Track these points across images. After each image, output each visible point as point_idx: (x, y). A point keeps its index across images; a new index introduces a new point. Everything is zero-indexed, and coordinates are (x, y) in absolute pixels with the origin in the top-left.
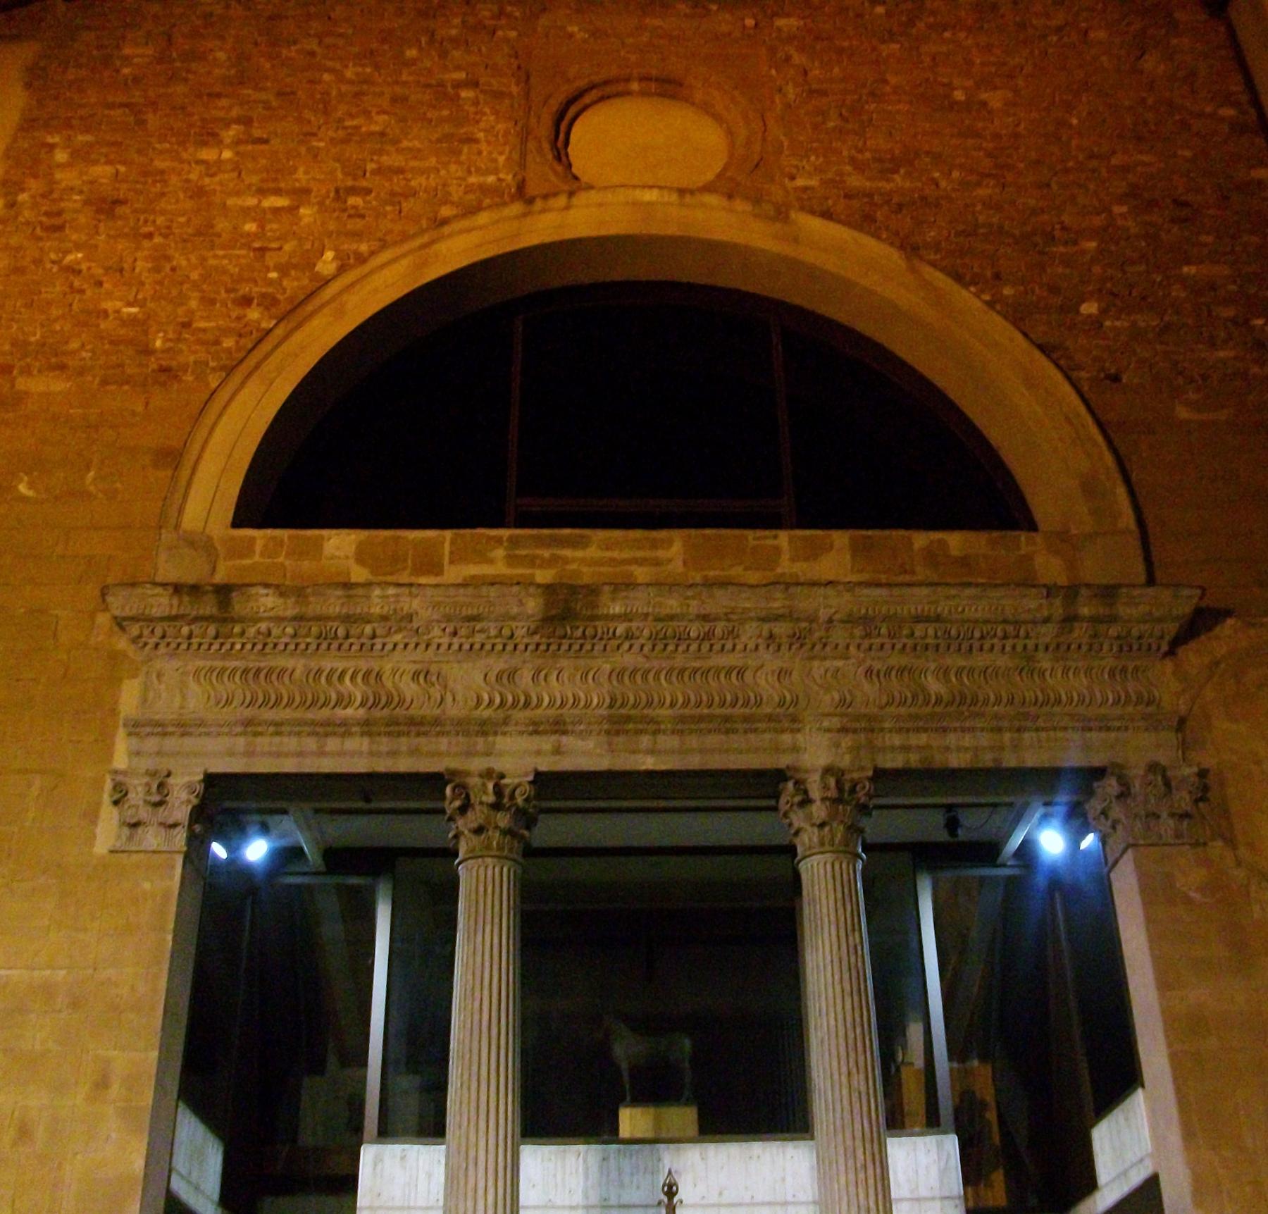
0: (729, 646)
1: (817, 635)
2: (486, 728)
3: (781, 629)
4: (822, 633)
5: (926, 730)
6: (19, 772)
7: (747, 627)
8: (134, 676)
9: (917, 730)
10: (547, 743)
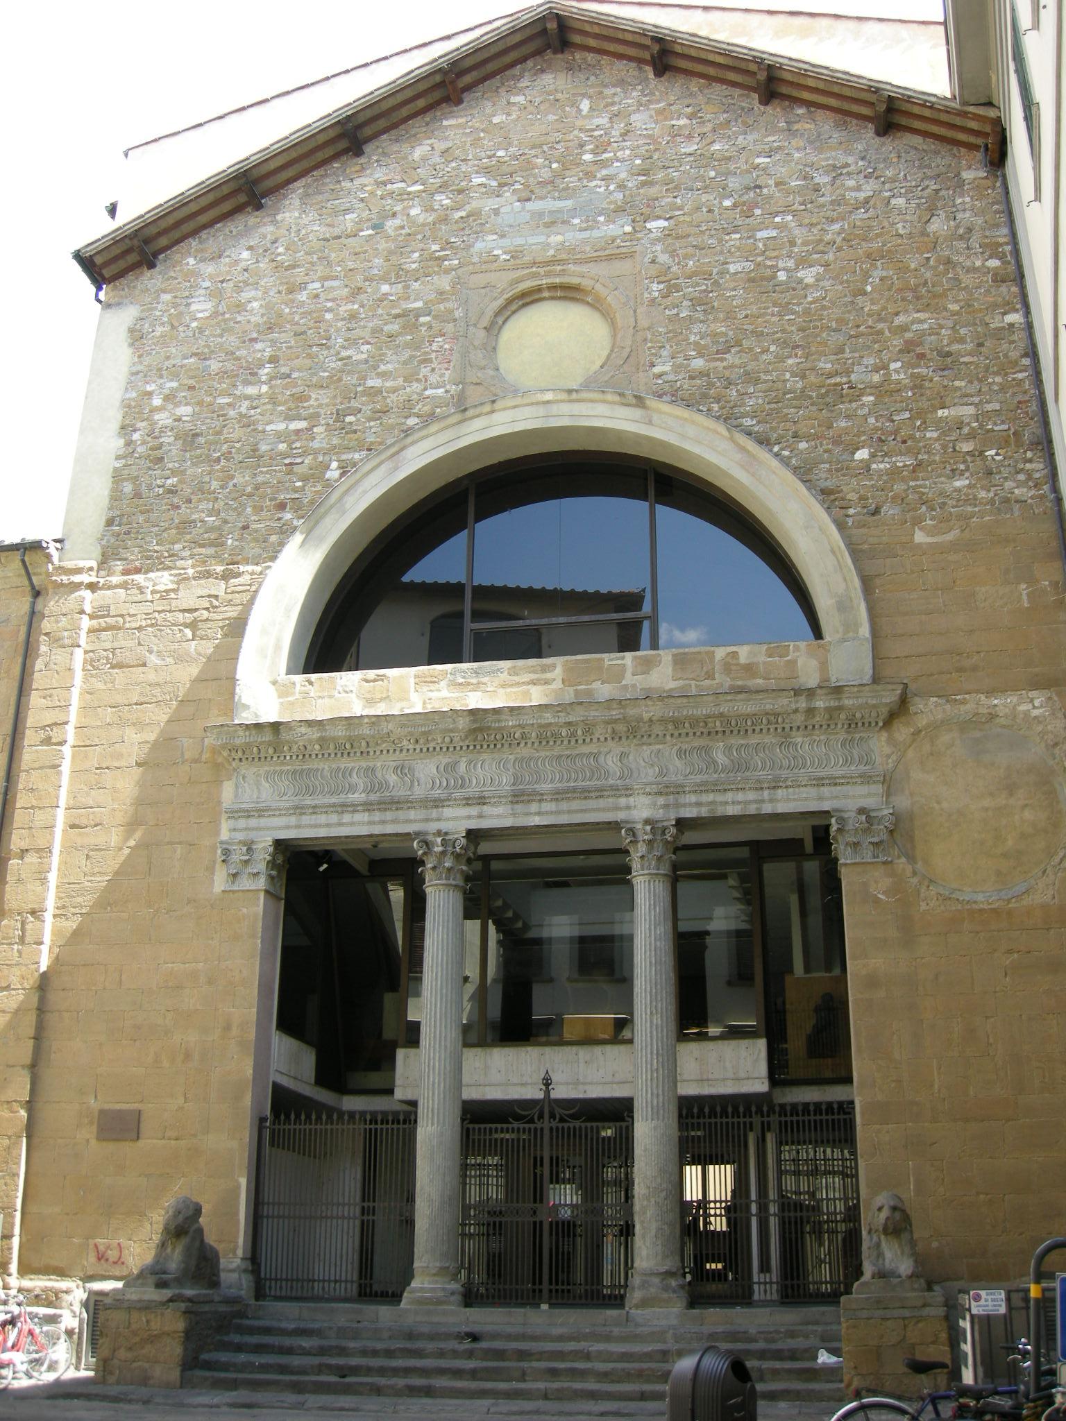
0: (588, 740)
2: (438, 803)
6: (168, 843)
10: (474, 811)
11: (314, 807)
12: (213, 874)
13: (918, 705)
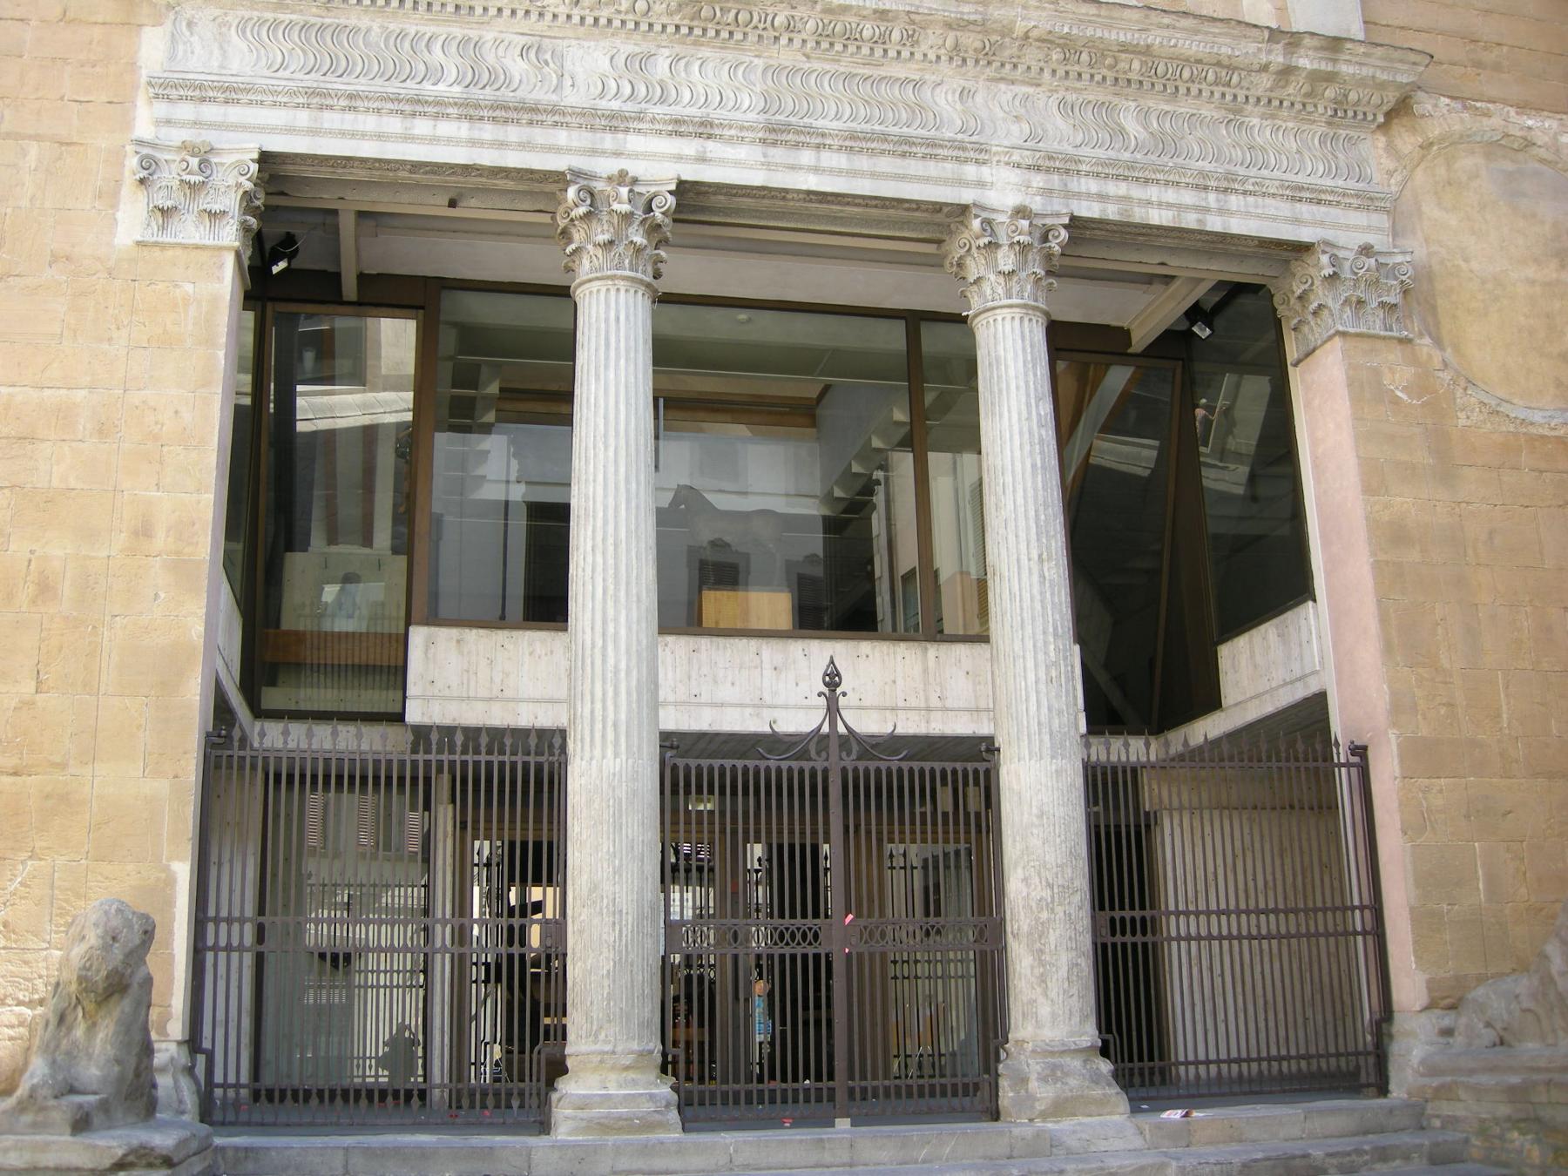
1: (1007, 53)
2: (615, 122)
3: (971, 41)
4: (1015, 51)
5: (1126, 179)
7: (930, 32)
8: (158, 23)
9: (1117, 177)
10: (690, 147)
11: (351, 97)
12: (115, 206)
13: (1422, 103)
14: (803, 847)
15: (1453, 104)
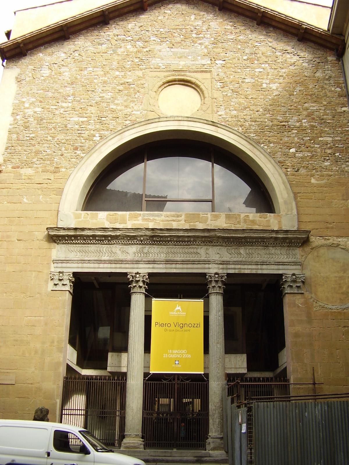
10: (151, 266)
12: (48, 284)
14: (263, 391)
15: (320, 238)
